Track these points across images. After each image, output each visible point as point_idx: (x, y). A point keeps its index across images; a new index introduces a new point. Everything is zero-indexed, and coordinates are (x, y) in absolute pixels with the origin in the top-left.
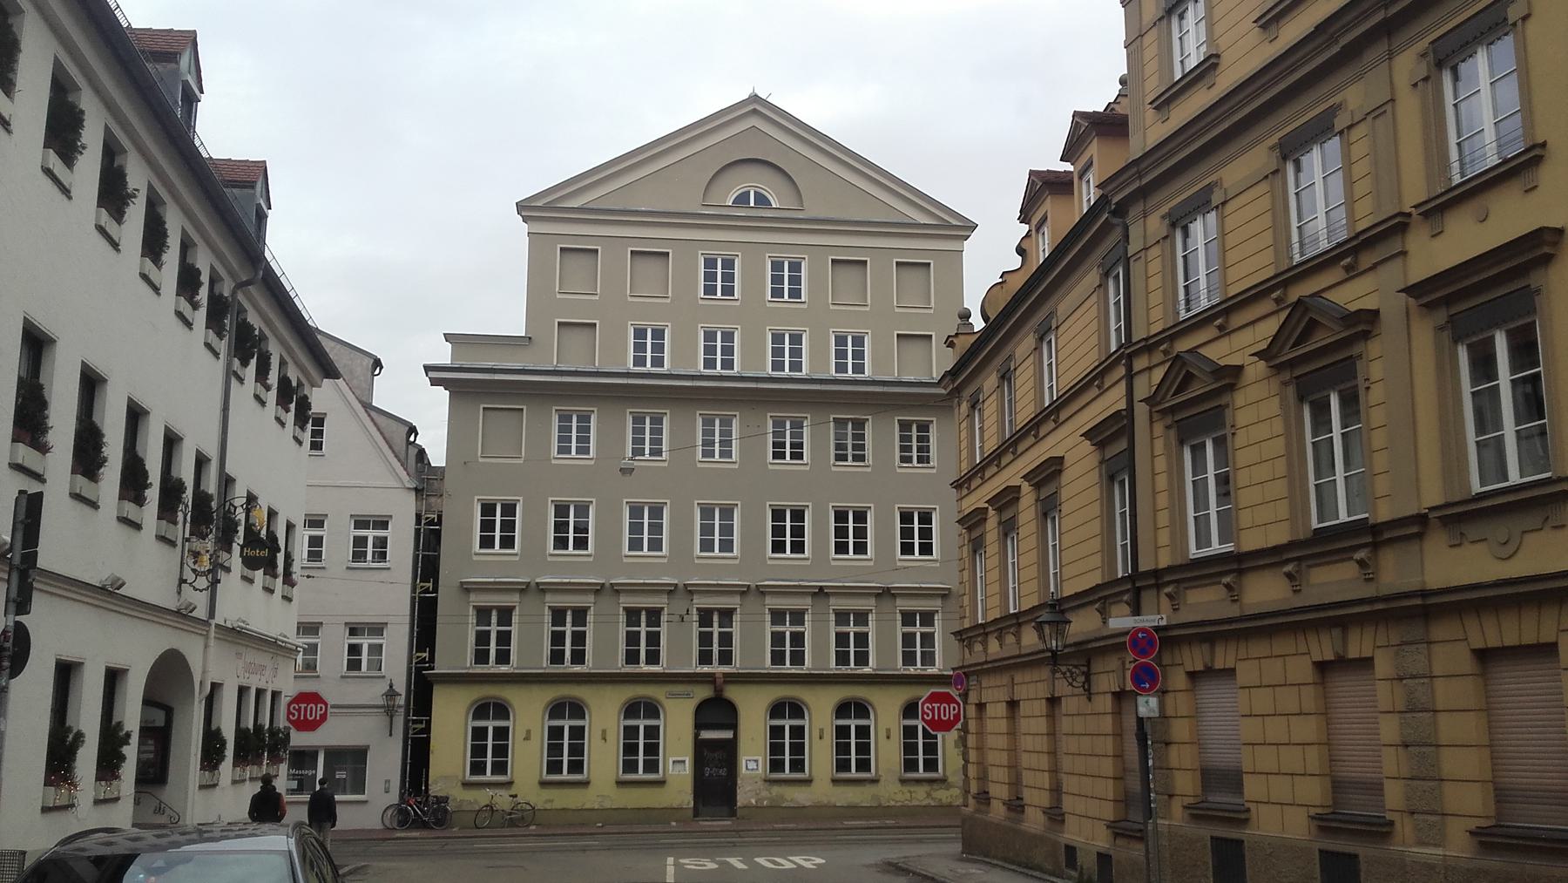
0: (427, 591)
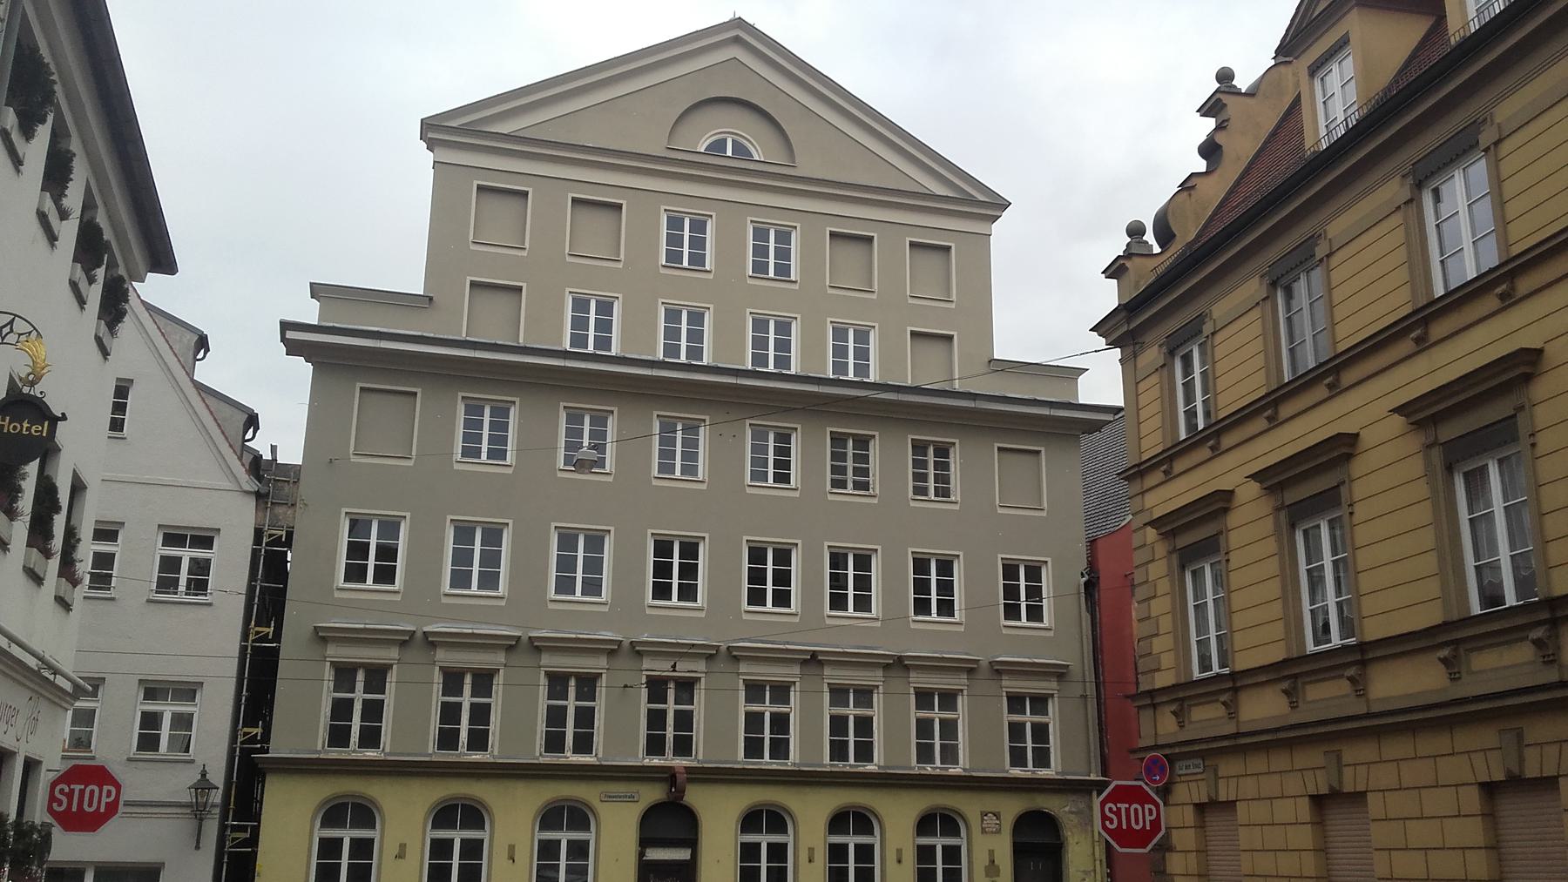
0: (264, 638)
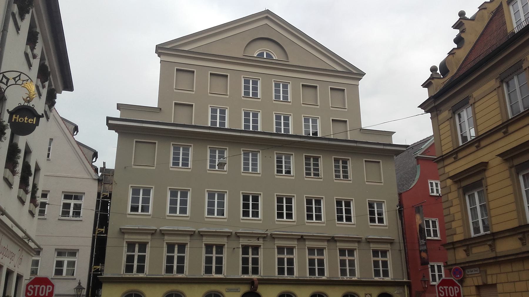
0: (101, 233)
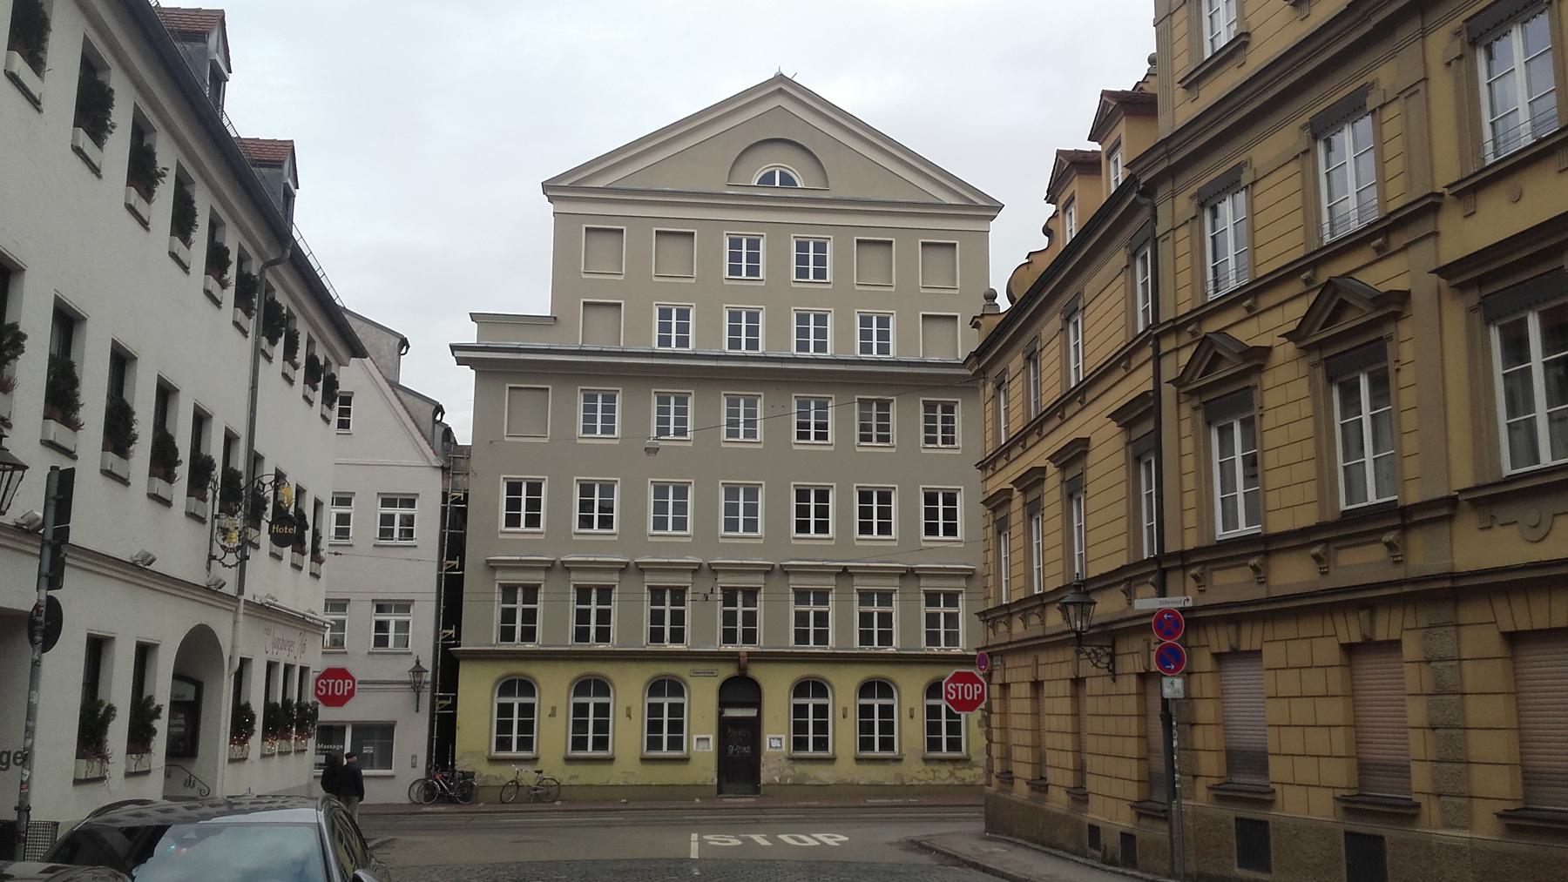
0: (453, 569)
